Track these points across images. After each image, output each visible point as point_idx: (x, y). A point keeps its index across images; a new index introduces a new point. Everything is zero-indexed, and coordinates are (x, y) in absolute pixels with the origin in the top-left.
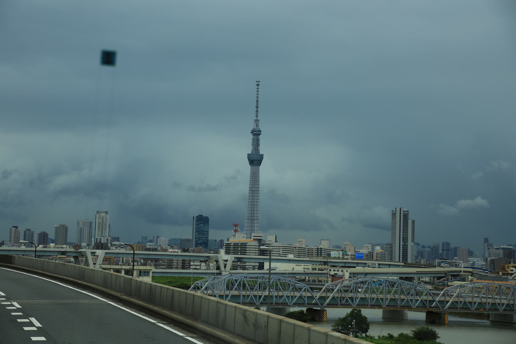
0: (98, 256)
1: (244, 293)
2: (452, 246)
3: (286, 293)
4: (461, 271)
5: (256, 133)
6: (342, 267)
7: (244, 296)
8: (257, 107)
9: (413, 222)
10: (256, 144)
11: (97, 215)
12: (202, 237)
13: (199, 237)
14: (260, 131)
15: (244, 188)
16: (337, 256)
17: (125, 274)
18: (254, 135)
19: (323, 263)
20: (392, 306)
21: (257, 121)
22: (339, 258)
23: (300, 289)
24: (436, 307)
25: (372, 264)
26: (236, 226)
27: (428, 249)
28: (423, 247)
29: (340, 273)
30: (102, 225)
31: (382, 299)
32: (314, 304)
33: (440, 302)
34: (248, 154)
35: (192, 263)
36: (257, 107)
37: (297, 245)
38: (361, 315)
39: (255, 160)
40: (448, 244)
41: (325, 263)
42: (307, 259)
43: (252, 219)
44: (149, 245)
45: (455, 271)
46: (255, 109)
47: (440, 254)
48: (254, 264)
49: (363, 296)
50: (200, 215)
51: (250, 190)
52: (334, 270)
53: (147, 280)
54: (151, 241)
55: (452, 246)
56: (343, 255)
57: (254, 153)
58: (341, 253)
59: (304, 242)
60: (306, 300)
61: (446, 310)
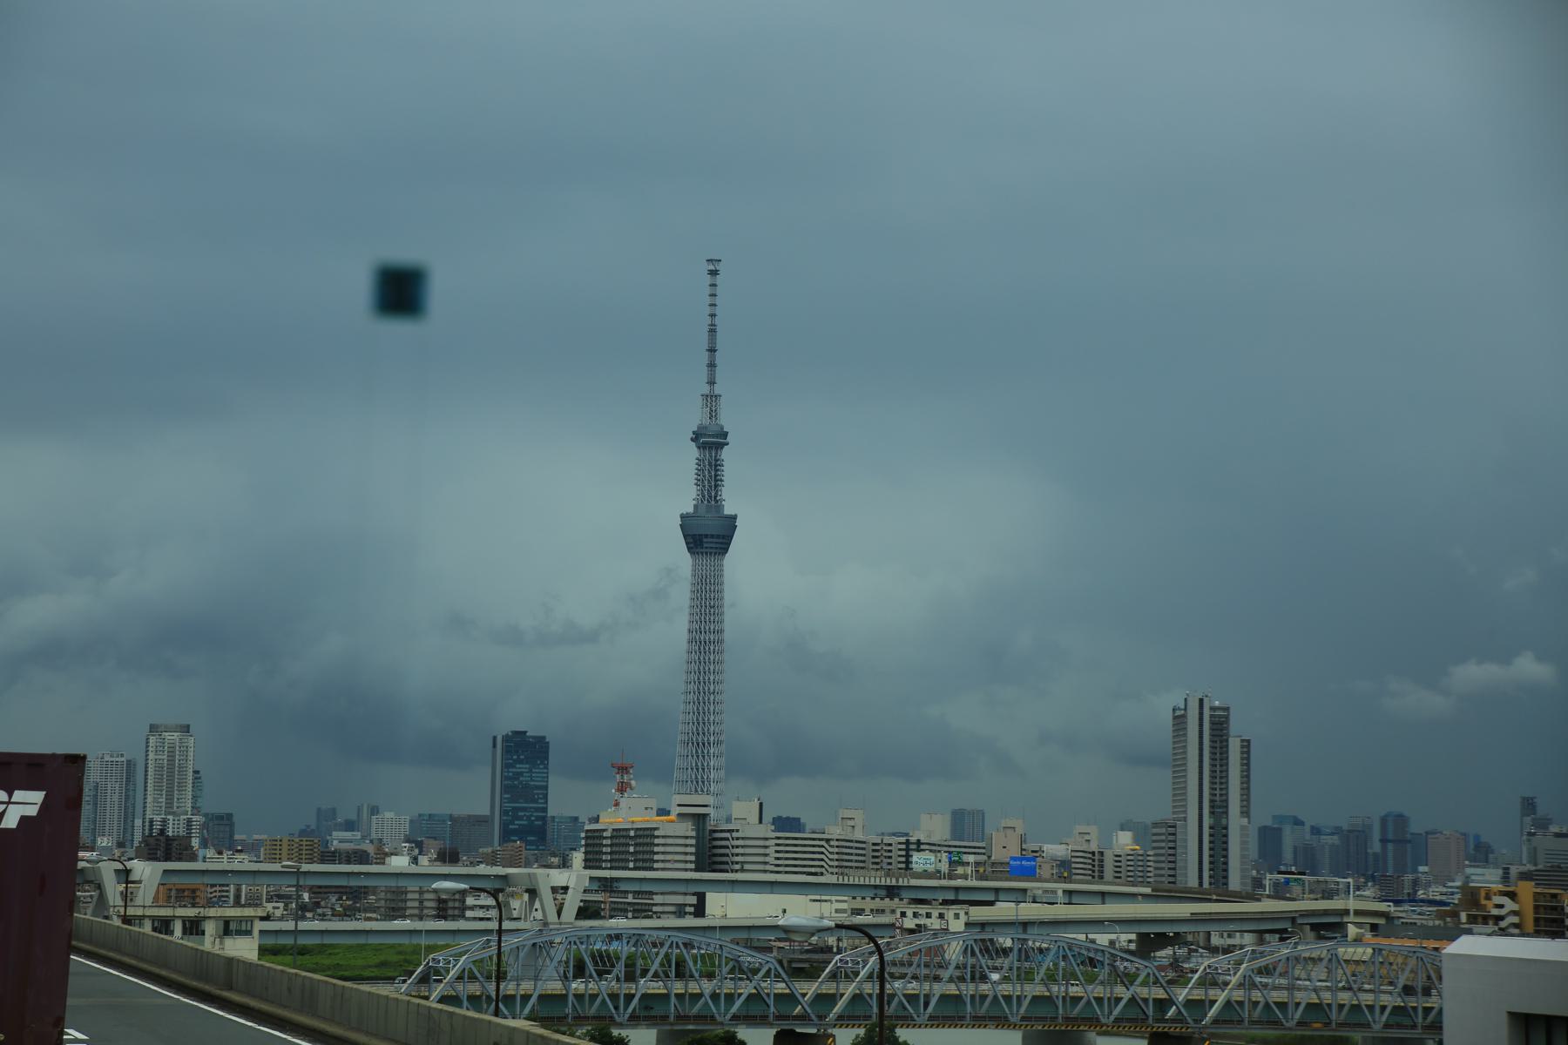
0: (140, 882)
1: (678, 987)
2: (1415, 827)
3: (707, 987)
4: (1347, 912)
5: (710, 442)
6: (945, 902)
7: (579, 997)
8: (712, 350)
9: (1246, 745)
10: (710, 478)
11: (152, 740)
12: (524, 809)
13: (515, 809)
14: (725, 435)
15: (675, 630)
16: (930, 868)
17: (154, 929)
18: (702, 447)
19: (883, 893)
20: (1038, 1019)
21: (711, 399)
22: (937, 874)
23: (755, 971)
24: (1179, 1019)
25: (1046, 891)
26: (623, 769)
27: (1335, 839)
28: (1316, 831)
29: (934, 923)
30: (170, 776)
31: (1008, 998)
32: (797, 1018)
33: (1189, 1003)
34: (683, 517)
35: (470, 901)
36: (712, 350)
37: (835, 832)
38: (896, 1039)
39: (708, 536)
40: (1401, 820)
41: (892, 892)
42: (833, 879)
43: (700, 741)
44: (339, 840)
45: (1326, 913)
46: (705, 357)
47: (1375, 854)
48: (679, 899)
49: (952, 989)
50: (517, 733)
51: (690, 642)
52: (915, 915)
53: (244, 949)
54: (350, 826)
55: (1415, 827)
56: (951, 863)
57: (702, 511)
58: (944, 856)
59: (859, 822)
60: (771, 1002)
61: (1205, 1027)
